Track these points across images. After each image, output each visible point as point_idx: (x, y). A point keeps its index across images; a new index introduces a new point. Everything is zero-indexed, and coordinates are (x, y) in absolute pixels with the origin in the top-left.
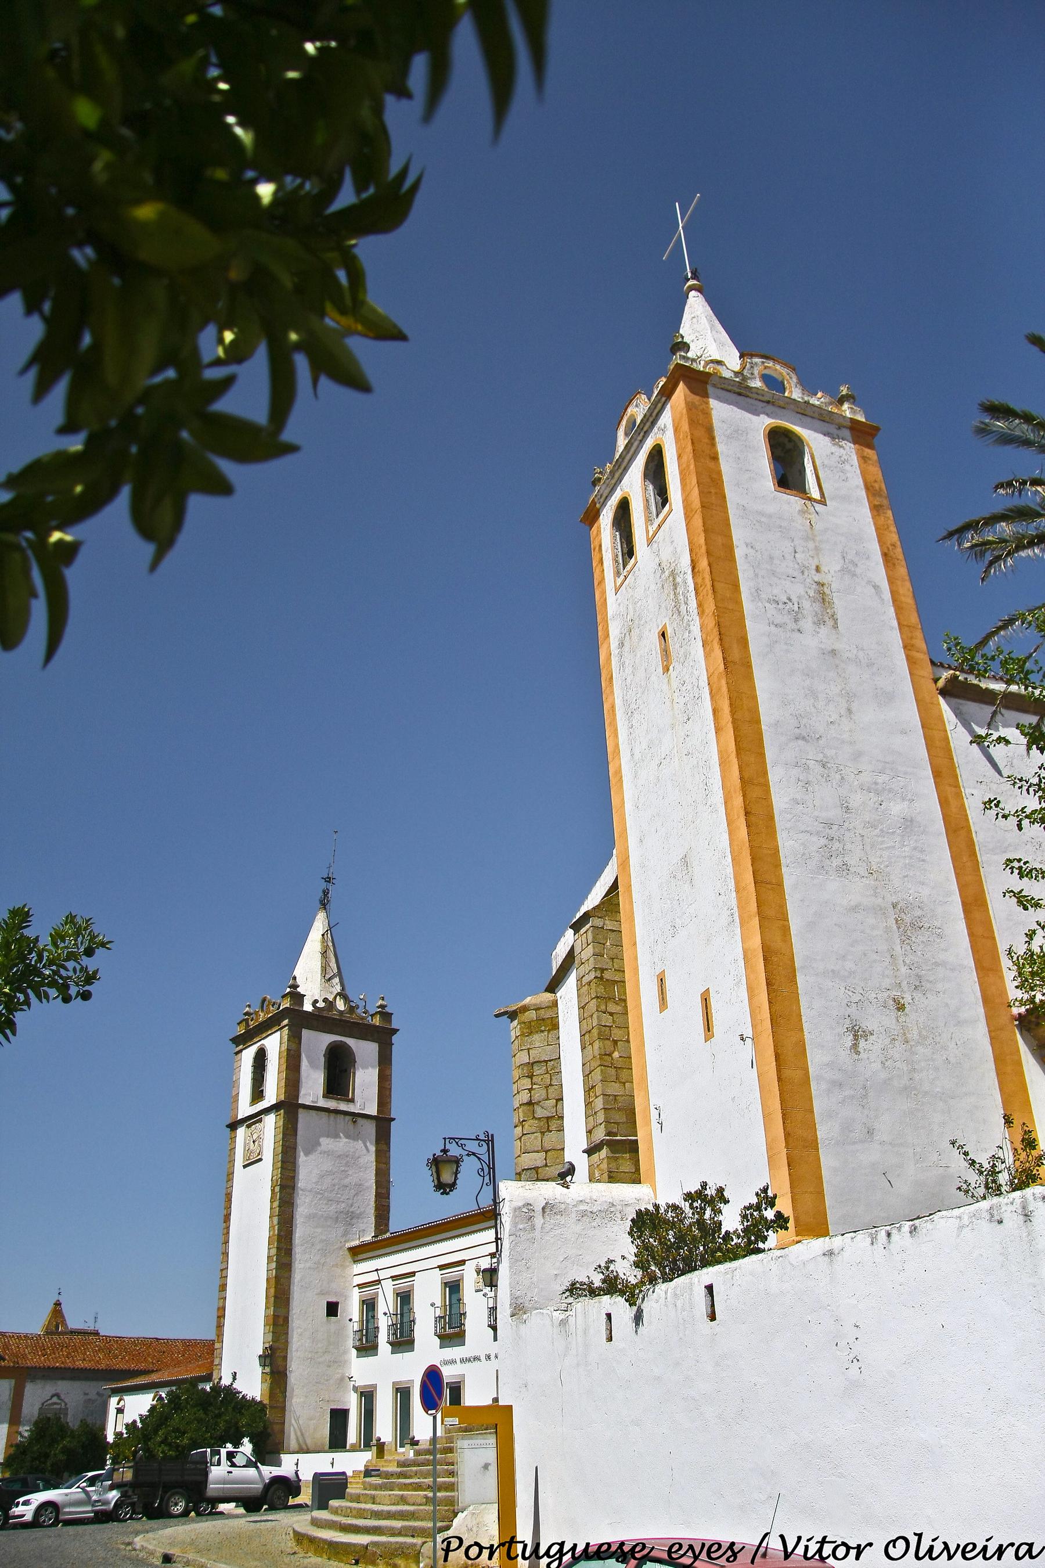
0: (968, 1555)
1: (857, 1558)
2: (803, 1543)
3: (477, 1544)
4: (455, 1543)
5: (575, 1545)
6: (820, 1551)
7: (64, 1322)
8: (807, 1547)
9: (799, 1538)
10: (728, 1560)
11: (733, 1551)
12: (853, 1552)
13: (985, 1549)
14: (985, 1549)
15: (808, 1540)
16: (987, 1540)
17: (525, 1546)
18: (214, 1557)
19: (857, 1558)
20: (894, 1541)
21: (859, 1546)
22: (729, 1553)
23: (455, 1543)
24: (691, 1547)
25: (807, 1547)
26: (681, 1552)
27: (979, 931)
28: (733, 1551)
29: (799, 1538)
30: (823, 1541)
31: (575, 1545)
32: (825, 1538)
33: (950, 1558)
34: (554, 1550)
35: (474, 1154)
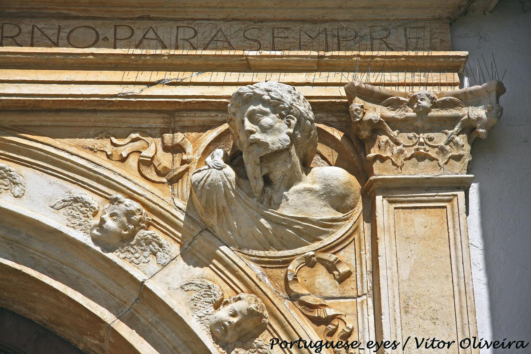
1: (448, 348)
6: (432, 345)
8: (427, 343)
9: (423, 339)
10: (393, 348)
11: (395, 344)
12: (446, 345)
13: (503, 343)
14: (503, 343)
19: (448, 348)
20: (464, 340)
21: (449, 342)
25: (427, 343)
26: (499, 345)
28: (395, 344)
29: (423, 339)
30: (434, 340)
32: (434, 339)
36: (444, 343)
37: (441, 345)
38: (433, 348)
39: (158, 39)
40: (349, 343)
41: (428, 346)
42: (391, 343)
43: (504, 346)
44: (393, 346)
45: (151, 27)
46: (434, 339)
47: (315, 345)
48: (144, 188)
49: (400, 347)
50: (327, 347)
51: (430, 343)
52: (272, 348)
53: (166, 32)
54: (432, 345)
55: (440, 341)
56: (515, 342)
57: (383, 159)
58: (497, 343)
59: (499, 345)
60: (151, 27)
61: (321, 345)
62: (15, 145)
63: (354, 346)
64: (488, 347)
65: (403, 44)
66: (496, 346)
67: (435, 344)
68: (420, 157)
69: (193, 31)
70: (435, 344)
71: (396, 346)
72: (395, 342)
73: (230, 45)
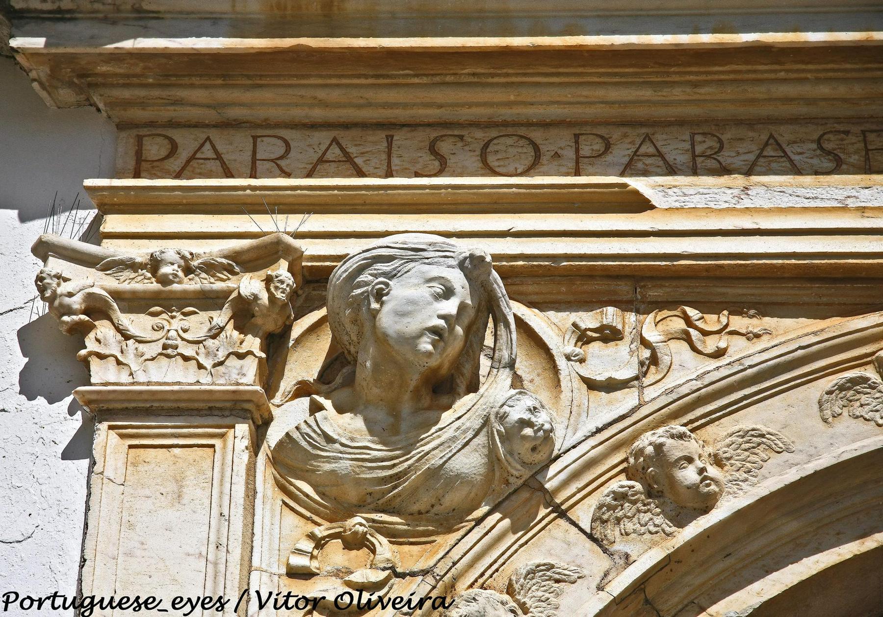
0: (206, 606)
1: (39, 608)
2: (274, 596)
3: (29, 597)
4: (12, 597)
5: (103, 599)
6: (286, 602)
7: (451, 316)
8: (276, 600)
9: (271, 593)
10: (134, 609)
11: (221, 603)
12: (36, 604)
13: (410, 601)
14: (410, 601)
15: (277, 595)
16: (412, 595)
17: (65, 599)
18: (528, 431)
19: (39, 608)
20: (342, 596)
21: (40, 599)
22: (218, 604)
23: (12, 597)
24: (189, 600)
25: (276, 600)
26: (402, 604)
27: (251, 478)
28: (221, 603)
29: (271, 593)
30: (289, 595)
31: (103, 599)
32: (290, 593)
33: (383, 608)
34: (88, 601)
35: (862, 416)
36: (32, 601)
37: (27, 603)
38: (288, 608)
39: (219, 157)
40: (141, 601)
41: (278, 606)
42: (215, 599)
43: (278, 606)
44: (135, 604)
45: (208, 139)
46: (290, 593)
47: (73, 603)
48: (789, 340)
49: (230, 607)
50: (102, 608)
51: (281, 601)
52: (6, 609)
53: (234, 147)
54: (286, 602)
55: (300, 596)
56: (48, 598)
57: (101, 357)
58: (179, 600)
59: (402, 604)
60: (208, 139)
61: (92, 603)
62: (793, 261)
63: (150, 606)
64: (383, 608)
65: (383, 173)
66: (206, 606)
67: (292, 602)
68: (168, 351)
69: (280, 143)
70: (292, 602)
71: (222, 606)
72: (221, 598)
73: (348, 159)
